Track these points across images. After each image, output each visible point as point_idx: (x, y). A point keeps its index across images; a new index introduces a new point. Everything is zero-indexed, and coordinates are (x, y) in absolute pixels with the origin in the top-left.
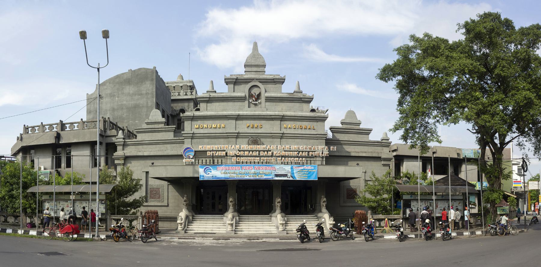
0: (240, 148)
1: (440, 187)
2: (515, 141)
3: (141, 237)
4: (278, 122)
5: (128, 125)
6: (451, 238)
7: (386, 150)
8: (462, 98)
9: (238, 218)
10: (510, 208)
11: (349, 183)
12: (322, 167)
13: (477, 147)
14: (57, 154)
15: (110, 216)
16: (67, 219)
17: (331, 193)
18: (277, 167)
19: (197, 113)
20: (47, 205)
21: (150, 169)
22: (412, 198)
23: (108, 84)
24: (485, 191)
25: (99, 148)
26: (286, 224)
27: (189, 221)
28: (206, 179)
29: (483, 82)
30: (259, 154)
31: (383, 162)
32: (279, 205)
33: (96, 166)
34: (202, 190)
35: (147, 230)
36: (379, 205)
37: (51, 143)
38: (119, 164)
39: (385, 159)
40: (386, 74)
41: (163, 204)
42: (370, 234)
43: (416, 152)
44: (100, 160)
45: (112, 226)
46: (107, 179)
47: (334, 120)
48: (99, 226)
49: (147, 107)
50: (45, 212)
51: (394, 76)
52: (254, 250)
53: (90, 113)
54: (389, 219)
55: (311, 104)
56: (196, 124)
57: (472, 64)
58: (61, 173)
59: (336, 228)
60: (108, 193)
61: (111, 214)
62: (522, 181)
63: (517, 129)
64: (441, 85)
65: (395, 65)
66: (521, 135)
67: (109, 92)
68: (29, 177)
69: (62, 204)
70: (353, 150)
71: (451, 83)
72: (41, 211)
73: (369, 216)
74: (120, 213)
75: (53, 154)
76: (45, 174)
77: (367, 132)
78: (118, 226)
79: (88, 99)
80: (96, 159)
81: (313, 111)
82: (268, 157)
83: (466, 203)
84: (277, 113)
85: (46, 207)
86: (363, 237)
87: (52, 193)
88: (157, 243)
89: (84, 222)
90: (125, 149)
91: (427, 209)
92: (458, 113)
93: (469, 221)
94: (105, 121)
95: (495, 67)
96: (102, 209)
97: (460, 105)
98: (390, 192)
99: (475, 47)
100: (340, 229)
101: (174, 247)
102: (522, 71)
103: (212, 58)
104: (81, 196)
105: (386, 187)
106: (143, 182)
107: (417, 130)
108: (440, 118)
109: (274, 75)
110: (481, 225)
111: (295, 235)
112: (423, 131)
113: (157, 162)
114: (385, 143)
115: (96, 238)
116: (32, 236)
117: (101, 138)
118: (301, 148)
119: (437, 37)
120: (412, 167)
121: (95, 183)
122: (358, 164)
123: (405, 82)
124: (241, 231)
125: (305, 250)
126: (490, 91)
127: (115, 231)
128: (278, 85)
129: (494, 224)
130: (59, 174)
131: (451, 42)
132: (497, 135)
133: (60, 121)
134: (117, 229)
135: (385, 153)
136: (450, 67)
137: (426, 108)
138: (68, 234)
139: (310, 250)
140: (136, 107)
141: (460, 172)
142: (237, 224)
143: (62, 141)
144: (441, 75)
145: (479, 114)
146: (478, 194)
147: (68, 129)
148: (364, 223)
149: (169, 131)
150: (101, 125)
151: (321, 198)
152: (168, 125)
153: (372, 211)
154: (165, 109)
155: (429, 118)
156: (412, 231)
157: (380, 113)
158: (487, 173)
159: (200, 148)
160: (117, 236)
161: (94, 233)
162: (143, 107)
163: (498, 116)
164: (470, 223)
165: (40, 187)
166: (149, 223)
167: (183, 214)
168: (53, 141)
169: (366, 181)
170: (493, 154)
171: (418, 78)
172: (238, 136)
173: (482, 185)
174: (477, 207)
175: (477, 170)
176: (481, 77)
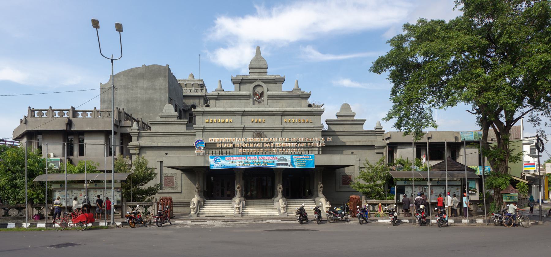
0: (246, 140)
1: (435, 173)
2: (527, 117)
3: (157, 222)
4: (280, 117)
6: (447, 225)
7: (380, 138)
8: (460, 79)
9: (244, 202)
10: (519, 195)
13: (478, 128)
14: (68, 141)
17: (328, 179)
18: (279, 157)
19: (207, 109)
20: (57, 194)
21: (164, 159)
22: (406, 184)
24: (488, 176)
25: (114, 138)
26: (287, 207)
27: (200, 206)
28: (215, 168)
29: (485, 57)
30: (263, 145)
31: (376, 150)
32: (280, 190)
33: (110, 154)
34: (212, 178)
35: (162, 215)
36: (373, 191)
38: (134, 154)
39: (379, 148)
40: (379, 66)
41: (176, 191)
43: (411, 138)
45: (128, 213)
47: (330, 112)
48: (114, 213)
50: (55, 202)
51: (387, 67)
52: (259, 230)
53: (104, 102)
54: (382, 204)
55: (309, 100)
56: (206, 119)
57: (471, 40)
58: (73, 161)
59: (332, 211)
60: (123, 181)
61: (127, 201)
62: (536, 163)
63: (529, 102)
64: (437, 68)
65: (389, 56)
66: (535, 108)
67: (123, 83)
68: (36, 165)
69: (75, 193)
70: (348, 140)
71: (448, 65)
72: (51, 201)
73: (363, 200)
74: (135, 200)
75: (64, 141)
76: (55, 162)
77: (361, 122)
78: (134, 213)
79: (101, 89)
80: (110, 149)
81: (310, 106)
82: (271, 148)
83: (464, 189)
84: (278, 109)
85: (57, 197)
87: (63, 182)
88: (171, 227)
89: (99, 210)
90: (140, 139)
91: (421, 194)
94: (119, 112)
95: (501, 35)
97: (458, 86)
98: (384, 178)
99: (476, 20)
100: (336, 212)
101: (188, 230)
102: (537, 31)
104: (96, 185)
105: (379, 174)
106: (157, 171)
107: (411, 117)
108: (436, 102)
109: (275, 76)
110: (483, 213)
112: (418, 117)
113: (171, 153)
114: (378, 132)
115: (111, 225)
116: (40, 229)
117: (116, 128)
119: (432, 21)
120: (406, 154)
121: (110, 172)
122: (352, 153)
123: (399, 71)
124: (248, 214)
125: (304, 230)
126: (495, 64)
127: (131, 218)
129: (499, 213)
130: (71, 162)
131: (447, 22)
132: (503, 112)
133: (72, 107)
134: (133, 215)
135: (379, 141)
136: (446, 49)
137: (420, 94)
138: (81, 223)
140: (150, 100)
141: (458, 156)
142: (244, 207)
144: (436, 59)
145: (479, 93)
146: (480, 180)
147: (80, 116)
148: (358, 207)
149: (181, 124)
150: (115, 115)
152: (180, 119)
154: (178, 104)
155: (424, 103)
157: (373, 104)
158: (491, 156)
159: (210, 140)
161: (109, 221)
163: (505, 91)
164: (469, 210)
165: (49, 175)
166: (164, 209)
167: (195, 200)
168: (64, 127)
169: (360, 168)
170: (498, 134)
171: (412, 65)
172: (244, 130)
173: (484, 170)
174: (478, 194)
175: (478, 153)
176: (483, 51)
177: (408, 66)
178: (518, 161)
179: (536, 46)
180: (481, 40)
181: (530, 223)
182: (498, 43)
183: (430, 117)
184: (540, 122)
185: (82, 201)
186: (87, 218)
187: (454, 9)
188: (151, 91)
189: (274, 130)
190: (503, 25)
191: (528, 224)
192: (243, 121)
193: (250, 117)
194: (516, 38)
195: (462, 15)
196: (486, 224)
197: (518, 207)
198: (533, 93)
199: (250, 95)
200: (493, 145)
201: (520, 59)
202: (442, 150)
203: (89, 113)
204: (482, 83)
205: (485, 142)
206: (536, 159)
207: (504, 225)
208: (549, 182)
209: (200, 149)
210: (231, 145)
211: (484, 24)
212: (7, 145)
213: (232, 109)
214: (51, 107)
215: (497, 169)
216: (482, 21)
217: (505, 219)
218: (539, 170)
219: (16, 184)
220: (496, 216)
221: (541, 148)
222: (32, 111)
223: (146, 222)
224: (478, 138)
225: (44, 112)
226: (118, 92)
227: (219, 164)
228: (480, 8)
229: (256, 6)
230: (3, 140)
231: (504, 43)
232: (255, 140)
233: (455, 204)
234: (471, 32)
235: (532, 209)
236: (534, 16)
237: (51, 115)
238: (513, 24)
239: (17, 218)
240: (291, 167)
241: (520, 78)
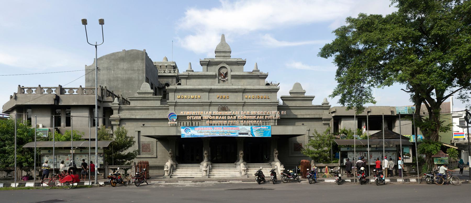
0: (212, 113)
1: (374, 140)
2: (456, 95)
3: (135, 182)
6: (384, 184)
7: (326, 112)
8: (395, 63)
9: (211, 166)
11: (296, 139)
12: (274, 127)
13: (412, 104)
14: (56, 114)
18: (240, 127)
19: (179, 87)
20: (45, 159)
21: (141, 129)
22: (349, 150)
24: (421, 143)
25: (98, 111)
27: (173, 169)
28: (186, 137)
29: (417, 45)
30: (227, 118)
31: (323, 122)
32: (242, 156)
34: (183, 145)
35: (140, 176)
36: (321, 156)
37: (50, 104)
38: (115, 125)
42: (313, 178)
43: (353, 112)
45: (110, 174)
47: (285, 90)
48: (98, 174)
50: (43, 165)
52: (223, 189)
54: (328, 167)
56: (178, 95)
57: (406, 31)
58: (61, 131)
60: (106, 148)
63: (458, 83)
64: (375, 54)
65: (334, 43)
66: (464, 88)
67: (106, 65)
69: (61, 158)
71: (385, 52)
72: (39, 164)
73: (312, 164)
74: (116, 163)
75: (52, 114)
76: (43, 131)
77: (311, 99)
78: (115, 174)
79: (86, 70)
80: (95, 120)
81: (268, 84)
82: (234, 120)
83: (399, 154)
84: (240, 87)
85: (45, 161)
86: (307, 181)
87: (51, 148)
88: (148, 186)
89: (84, 172)
90: (120, 113)
92: (392, 76)
93: (403, 169)
94: (102, 89)
95: (432, 28)
96: (101, 161)
97: (394, 69)
99: (409, 15)
100: (289, 174)
101: (162, 189)
102: (466, 25)
103: (189, 45)
104: (81, 151)
105: (326, 142)
106: (136, 139)
107: (353, 94)
108: (374, 82)
109: (238, 59)
110: (416, 174)
111: (254, 178)
112: (359, 94)
113: (147, 124)
114: (325, 107)
115: (95, 185)
116: (29, 188)
117: (99, 103)
118: (259, 113)
119: (371, 15)
121: (94, 140)
122: (303, 124)
125: (262, 189)
126: (426, 52)
127: (112, 178)
129: (430, 173)
130: (59, 131)
131: (384, 16)
132: (434, 91)
133: (60, 85)
134: (114, 177)
135: (325, 114)
136: (383, 38)
138: (68, 183)
139: (265, 189)
140: (129, 80)
141: (394, 127)
142: (210, 170)
143: (63, 103)
144: (374, 46)
145: (413, 75)
146: (413, 146)
147: (67, 93)
148: (308, 169)
149: (156, 100)
150: (98, 92)
151: (274, 150)
152: (156, 95)
155: (364, 83)
156: (348, 177)
157: (321, 83)
158: (423, 126)
159: (182, 113)
160: (114, 182)
161: (93, 181)
162: (135, 80)
163: (436, 73)
164: (404, 171)
165: (37, 142)
167: (169, 164)
168: (52, 102)
169: (310, 137)
171: (354, 52)
172: (210, 104)
173: (417, 138)
174: (411, 158)
177: (351, 52)
179: (464, 38)
180: (414, 32)
181: (460, 182)
182: (430, 34)
183: (370, 94)
184: (469, 99)
187: (390, 6)
188: (130, 71)
189: (236, 105)
190: (434, 19)
191: (458, 183)
192: (210, 97)
193: (216, 94)
194: (445, 30)
195: (397, 11)
196: (419, 182)
197: (448, 168)
200: (425, 118)
201: (449, 47)
202: (382, 122)
203: (75, 90)
204: (415, 67)
207: (435, 183)
210: (200, 117)
211: (416, 18)
213: (201, 87)
215: (429, 137)
217: (436, 178)
219: (5, 150)
220: (428, 176)
222: (21, 89)
223: (126, 182)
226: (101, 72)
227: (190, 134)
228: (413, 6)
232: (220, 113)
233: (391, 166)
234: (406, 25)
235: (462, 170)
236: (464, 13)
238: (443, 19)
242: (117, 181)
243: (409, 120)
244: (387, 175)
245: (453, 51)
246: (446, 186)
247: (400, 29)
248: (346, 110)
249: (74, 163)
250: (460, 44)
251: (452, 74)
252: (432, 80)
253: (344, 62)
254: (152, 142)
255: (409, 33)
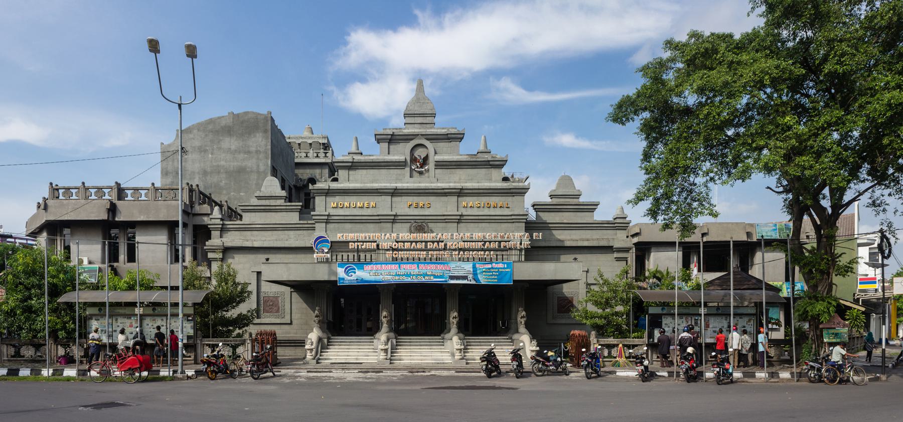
0: (398, 238)
1: (714, 293)
2: (865, 199)
3: (251, 372)
5: (229, 198)
6: (732, 382)
7: (622, 235)
8: (757, 133)
9: (394, 341)
10: (850, 331)
13: (785, 218)
14: (110, 238)
15: (201, 341)
16: (131, 346)
17: (537, 304)
18: (452, 265)
19: (334, 185)
20: (94, 324)
21: (263, 268)
22: (665, 312)
23: (195, 131)
24: (800, 298)
25: (183, 233)
27: (323, 346)
28: (347, 283)
29: (798, 96)
30: (426, 246)
31: (616, 255)
32: (455, 321)
33: (177, 260)
34: (342, 300)
35: (260, 360)
36: (609, 323)
37: (100, 218)
38: (215, 260)
39: (620, 250)
40: (622, 112)
41: (283, 321)
43: (673, 235)
44: (183, 251)
45: (205, 355)
46: (196, 282)
47: (540, 191)
48: (184, 356)
49: (258, 172)
50: (91, 336)
51: (636, 113)
52: (418, 387)
54: (624, 345)
56: (333, 201)
57: (777, 67)
58: (119, 270)
60: (198, 304)
61: (204, 337)
62: (879, 277)
63: (869, 174)
65: (639, 95)
66: (879, 184)
67: (197, 143)
68: (61, 276)
69: (121, 323)
70: (568, 238)
71: (737, 110)
72: (84, 335)
73: (593, 339)
74: (217, 335)
75: (104, 238)
76: (90, 271)
77: (591, 207)
78: (214, 356)
79: (163, 152)
80: (177, 251)
81: (505, 179)
82: (439, 250)
84: (452, 185)
85: (94, 328)
86: (582, 372)
87: (103, 304)
88: (275, 380)
89: (160, 350)
90: (224, 235)
91: (689, 329)
93: (767, 353)
94: (191, 190)
95: (825, 59)
96: (189, 329)
97: (754, 145)
98: (627, 302)
99: (785, 33)
100: (548, 359)
101: (301, 385)
102: (883, 52)
104: (154, 310)
106: (252, 288)
107: (675, 198)
108: (716, 173)
110: (790, 362)
111: (478, 366)
112: (686, 198)
113: (274, 258)
114: (619, 224)
115: (179, 375)
116: (69, 379)
117: (186, 217)
119: (712, 34)
121: (177, 288)
123: (655, 120)
125: (494, 388)
126: (814, 109)
127: (209, 363)
128: (453, 143)
129: (816, 361)
130: (115, 271)
131: (737, 37)
132: (826, 191)
133: (116, 183)
134: (213, 360)
135: (620, 239)
137: (690, 159)
138: (132, 371)
139: (500, 388)
140: (241, 171)
141: (752, 265)
142: (394, 349)
143: (120, 218)
144: (718, 99)
145: (788, 158)
146: (786, 305)
147: (129, 198)
148: (584, 350)
149: (291, 211)
150: (184, 195)
152: (290, 201)
153: (598, 331)
154: (286, 177)
156: (663, 366)
157: (611, 179)
158: (805, 265)
159: (339, 237)
161: (175, 368)
163: (830, 154)
164: (768, 357)
167: (314, 336)
168: (103, 216)
169: (588, 285)
170: (817, 228)
171: (678, 110)
172: (395, 220)
173: (793, 288)
174: (782, 329)
175: (784, 260)
176: (796, 85)
177: (672, 112)
178: (849, 274)
179: (882, 78)
181: (866, 378)
182: (821, 72)
183: (707, 198)
185: (133, 336)
186: (141, 363)
187: (748, 15)
190: (829, 41)
191: (863, 380)
192: (394, 205)
193: (405, 199)
194: (850, 64)
196: (796, 379)
198: (873, 158)
199: (406, 161)
200: (808, 247)
201: (855, 100)
202: (724, 256)
204: (793, 142)
205: (797, 242)
206: (879, 271)
207: (823, 381)
208: (899, 309)
209: (323, 252)
211: (798, 40)
212: (17, 244)
213: (376, 185)
214: (83, 183)
216: (795, 35)
217: (827, 371)
218: (883, 288)
220: (812, 367)
221: (887, 252)
223: (235, 371)
224: (785, 235)
225: (74, 191)
226: (189, 157)
227: (354, 277)
228: (792, 13)
229: (417, 12)
230: (11, 237)
231: (830, 72)
233: (745, 345)
234: (777, 54)
235: (870, 354)
237: (84, 196)
239: (33, 361)
240: (473, 282)
241: (855, 133)
242: (219, 367)
243: (780, 252)
244: (736, 364)
245: (861, 107)
246: (842, 386)
247: (766, 62)
248: (661, 230)
249: (142, 333)
250: (873, 92)
251: (859, 154)
252: (823, 169)
253: (658, 133)
254: (283, 294)
255: (783, 71)
